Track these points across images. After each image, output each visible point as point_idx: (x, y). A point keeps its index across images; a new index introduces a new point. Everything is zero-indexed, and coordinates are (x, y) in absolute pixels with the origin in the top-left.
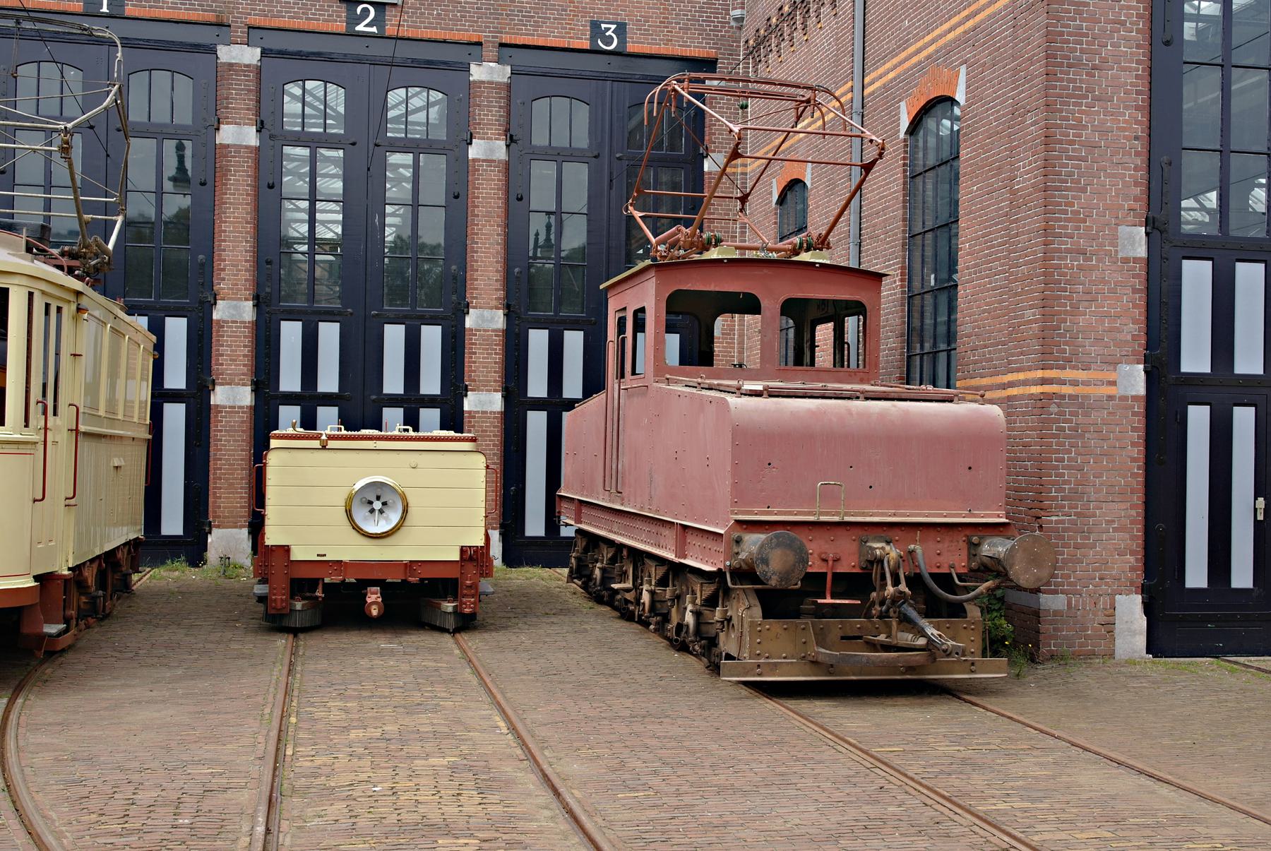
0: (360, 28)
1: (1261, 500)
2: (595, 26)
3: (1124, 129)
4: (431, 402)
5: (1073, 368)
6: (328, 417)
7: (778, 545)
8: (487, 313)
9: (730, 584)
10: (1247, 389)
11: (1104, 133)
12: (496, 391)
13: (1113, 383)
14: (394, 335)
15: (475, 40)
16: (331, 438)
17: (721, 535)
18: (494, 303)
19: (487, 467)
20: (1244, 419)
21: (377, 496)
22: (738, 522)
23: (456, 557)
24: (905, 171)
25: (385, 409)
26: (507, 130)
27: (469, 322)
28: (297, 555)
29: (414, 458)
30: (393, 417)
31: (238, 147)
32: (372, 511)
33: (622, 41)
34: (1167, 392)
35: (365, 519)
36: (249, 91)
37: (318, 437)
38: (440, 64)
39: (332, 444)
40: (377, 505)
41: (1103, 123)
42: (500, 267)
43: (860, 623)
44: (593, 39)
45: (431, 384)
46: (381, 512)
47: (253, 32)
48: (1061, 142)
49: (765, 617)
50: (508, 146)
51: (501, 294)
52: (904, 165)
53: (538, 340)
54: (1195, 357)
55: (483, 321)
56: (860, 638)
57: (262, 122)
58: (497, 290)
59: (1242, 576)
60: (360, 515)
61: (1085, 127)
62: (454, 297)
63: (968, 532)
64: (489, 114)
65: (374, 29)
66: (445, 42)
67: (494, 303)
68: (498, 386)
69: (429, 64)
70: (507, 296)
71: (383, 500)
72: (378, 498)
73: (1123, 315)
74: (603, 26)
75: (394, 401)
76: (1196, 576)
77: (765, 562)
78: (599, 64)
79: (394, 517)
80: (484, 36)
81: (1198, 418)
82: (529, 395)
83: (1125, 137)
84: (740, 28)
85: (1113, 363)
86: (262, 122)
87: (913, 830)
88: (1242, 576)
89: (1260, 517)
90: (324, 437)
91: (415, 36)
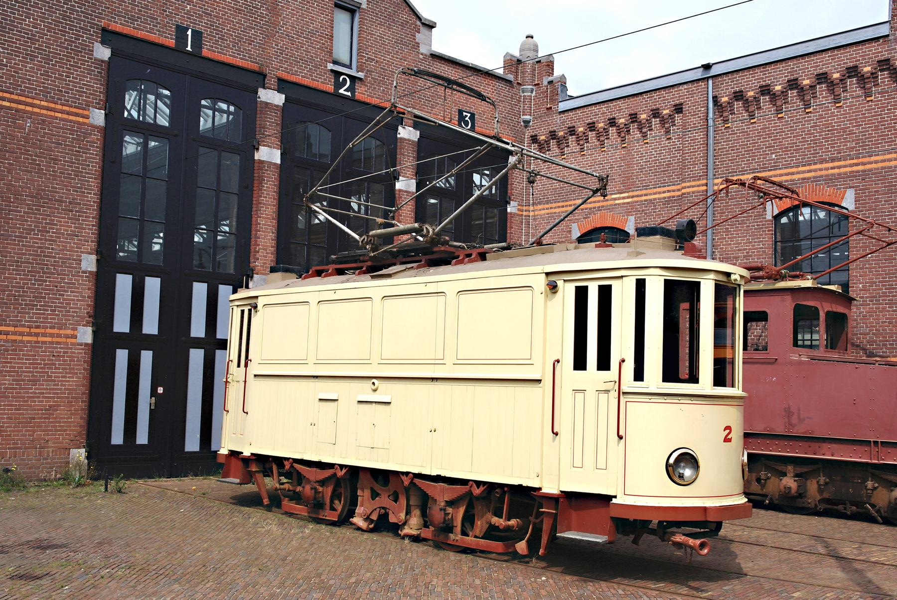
0: (341, 91)
10: (148, 342)
14: (200, 290)
20: (147, 357)
31: (270, 163)
34: (105, 342)
36: (277, 124)
38: (240, 84)
47: (283, 85)
54: (122, 324)
59: (142, 438)
65: (349, 94)
73: (81, 298)
76: (117, 438)
81: (122, 356)
87: (858, 566)
88: (142, 438)
89: (153, 408)
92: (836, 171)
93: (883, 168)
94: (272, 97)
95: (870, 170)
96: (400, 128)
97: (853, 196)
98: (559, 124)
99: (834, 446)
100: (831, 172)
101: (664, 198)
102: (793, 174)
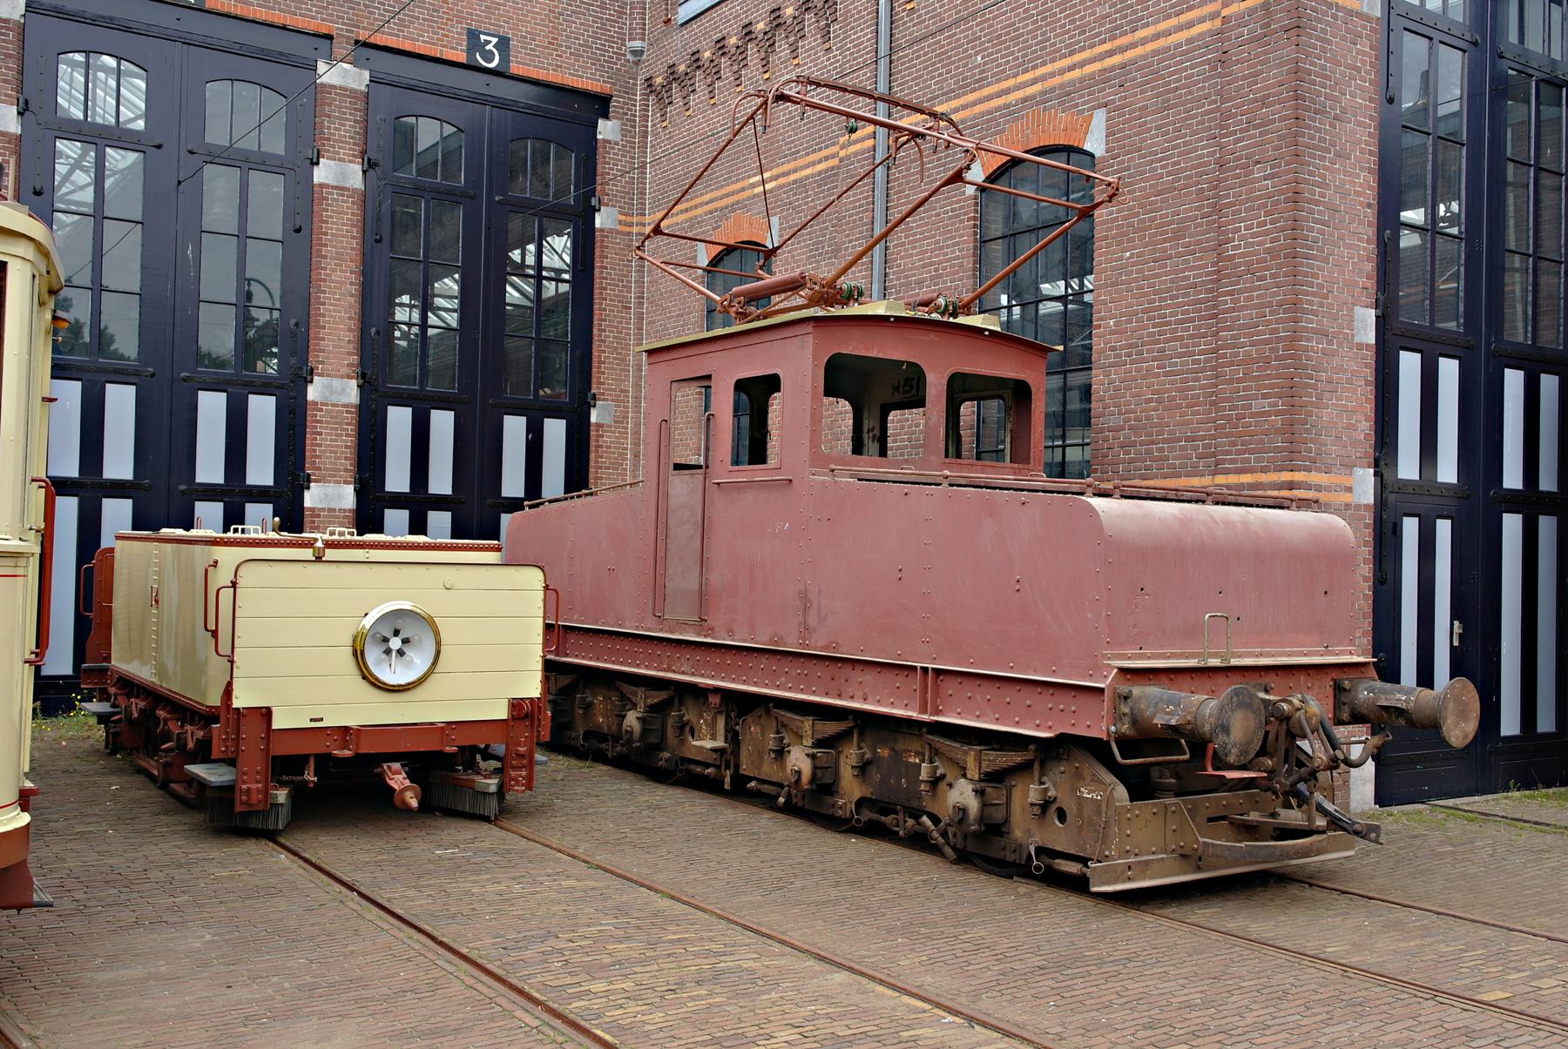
1: (1456, 623)
2: (473, 35)
3: (1358, 194)
4: (260, 495)
5: (1318, 470)
6: (440, 520)
7: (1239, 705)
8: (337, 383)
9: (1119, 758)
11: (1344, 195)
12: (346, 482)
13: (1349, 489)
15: (325, 31)
16: (330, 545)
17: (1102, 690)
18: (345, 370)
19: (546, 588)
21: (399, 629)
22: (1123, 670)
23: (502, 713)
24: (975, 234)
25: (197, 504)
26: (364, 152)
27: (313, 393)
28: (278, 723)
29: (450, 574)
30: (209, 513)
32: (388, 652)
33: (505, 59)
35: (379, 662)
37: (309, 544)
38: (282, 56)
39: (330, 554)
40: (395, 643)
41: (1343, 182)
42: (353, 324)
43: (1225, 798)
44: (471, 50)
45: (260, 472)
46: (401, 653)
48: (1310, 201)
49: (1132, 799)
50: (364, 172)
51: (355, 359)
52: (975, 226)
53: (399, 420)
55: (332, 393)
56: (1223, 818)
57: (26, 102)
58: (349, 354)
60: (373, 656)
61: (1328, 187)
62: (293, 360)
63: (1335, 674)
64: (342, 128)
66: (284, 28)
67: (345, 370)
68: (350, 477)
69: (264, 56)
70: (362, 363)
71: (403, 635)
72: (396, 633)
74: (483, 37)
75: (210, 493)
77: (1226, 729)
78: (476, 83)
79: (418, 663)
80: (335, 28)
82: (388, 489)
83: (1361, 203)
84: (637, 63)
85: (1349, 466)
86: (26, 102)
89: (1456, 643)
90: (319, 544)
91: (245, 14)
92: (1076, 73)
93: (1155, 53)
94: (341, 75)
95: (1133, 62)
96: (322, 67)
97: (1103, 125)
98: (677, 48)
99: (869, 676)
100: (1069, 76)
101: (820, 173)
102: (1007, 91)
